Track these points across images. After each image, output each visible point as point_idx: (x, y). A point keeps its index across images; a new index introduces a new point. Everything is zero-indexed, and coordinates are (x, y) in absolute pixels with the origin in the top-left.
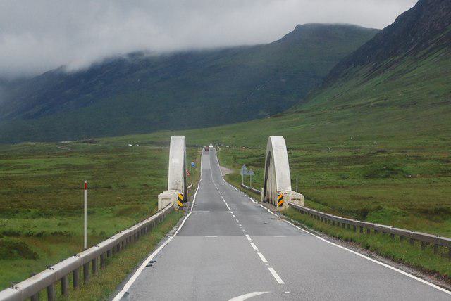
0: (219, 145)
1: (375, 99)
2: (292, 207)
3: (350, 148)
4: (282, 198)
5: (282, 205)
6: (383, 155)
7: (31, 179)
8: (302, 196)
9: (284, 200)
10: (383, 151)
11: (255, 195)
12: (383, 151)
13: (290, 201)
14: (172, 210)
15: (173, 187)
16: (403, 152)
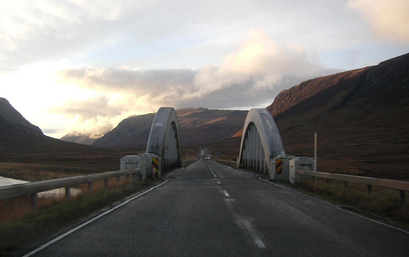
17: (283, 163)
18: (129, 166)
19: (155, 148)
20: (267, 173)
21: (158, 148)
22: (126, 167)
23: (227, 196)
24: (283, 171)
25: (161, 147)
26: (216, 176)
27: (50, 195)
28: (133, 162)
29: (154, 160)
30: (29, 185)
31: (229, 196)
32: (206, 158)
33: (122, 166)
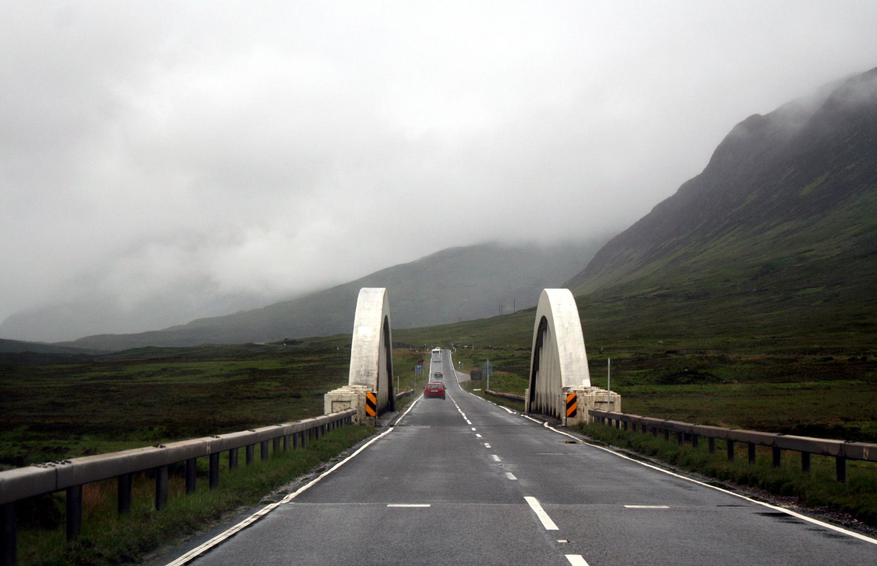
0: (571, 527)
1: (654, 288)
2: (598, 417)
3: (629, 348)
4: (574, 400)
5: (573, 414)
6: (674, 356)
7: (149, 381)
8: (617, 396)
9: (580, 403)
10: (674, 352)
11: (515, 403)
12: (674, 352)
13: (591, 406)
14: (343, 421)
15: (359, 380)
16: (701, 353)
17: (578, 400)
18: (337, 406)
19: (364, 375)
20: (559, 418)
21: (370, 374)
22: (332, 409)
23: (548, 528)
24: (578, 412)
25: (374, 374)
26: (486, 444)
27: (681, 344)
28: (344, 399)
29: (369, 397)
30: (191, 439)
31: (556, 528)
32: (472, 431)
33: (327, 407)
